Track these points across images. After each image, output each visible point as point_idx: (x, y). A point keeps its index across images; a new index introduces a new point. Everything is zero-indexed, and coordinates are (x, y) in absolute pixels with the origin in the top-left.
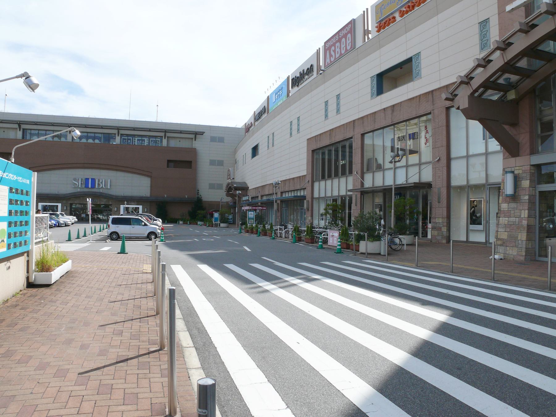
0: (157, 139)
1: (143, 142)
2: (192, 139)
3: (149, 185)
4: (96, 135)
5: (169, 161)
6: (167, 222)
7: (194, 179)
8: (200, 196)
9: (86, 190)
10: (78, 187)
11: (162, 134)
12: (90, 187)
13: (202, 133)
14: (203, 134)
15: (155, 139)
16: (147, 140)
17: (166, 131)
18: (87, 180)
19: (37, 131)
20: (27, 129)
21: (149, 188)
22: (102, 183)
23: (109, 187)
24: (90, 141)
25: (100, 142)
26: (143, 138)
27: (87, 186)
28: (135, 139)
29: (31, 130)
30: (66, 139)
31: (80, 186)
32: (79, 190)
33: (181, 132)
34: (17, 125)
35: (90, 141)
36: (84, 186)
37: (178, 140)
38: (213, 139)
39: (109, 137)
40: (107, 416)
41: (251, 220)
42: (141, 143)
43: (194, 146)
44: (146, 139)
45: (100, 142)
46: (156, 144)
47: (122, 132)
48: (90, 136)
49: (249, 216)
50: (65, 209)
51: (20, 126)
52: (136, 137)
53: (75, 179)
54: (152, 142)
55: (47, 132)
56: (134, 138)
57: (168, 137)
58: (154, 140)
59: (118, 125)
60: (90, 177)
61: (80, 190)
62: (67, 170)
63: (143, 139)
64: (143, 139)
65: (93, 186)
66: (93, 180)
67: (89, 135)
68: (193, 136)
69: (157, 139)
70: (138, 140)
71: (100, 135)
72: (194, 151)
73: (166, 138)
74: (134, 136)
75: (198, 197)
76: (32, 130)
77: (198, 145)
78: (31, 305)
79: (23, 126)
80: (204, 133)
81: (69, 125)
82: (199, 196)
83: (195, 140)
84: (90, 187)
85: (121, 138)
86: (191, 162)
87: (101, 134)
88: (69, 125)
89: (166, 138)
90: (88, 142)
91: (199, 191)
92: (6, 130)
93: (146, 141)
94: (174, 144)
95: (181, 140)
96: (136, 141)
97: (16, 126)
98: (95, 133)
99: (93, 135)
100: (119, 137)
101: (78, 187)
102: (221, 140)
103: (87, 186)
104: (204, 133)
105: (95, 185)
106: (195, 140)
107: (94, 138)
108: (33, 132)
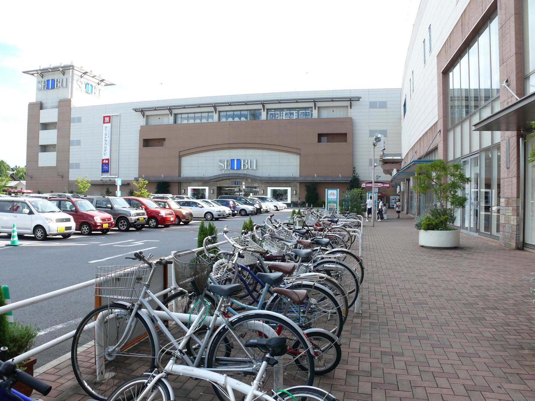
0: (306, 111)
1: (292, 116)
2: (347, 107)
3: (298, 164)
4: (242, 112)
5: (320, 136)
6: (293, 206)
7: (351, 155)
8: (357, 174)
9: (232, 172)
10: (224, 169)
11: (312, 105)
12: (236, 168)
13: (358, 99)
14: (359, 100)
15: (305, 111)
16: (296, 113)
17: (315, 101)
18: (232, 161)
19: (207, 114)
20: (178, 114)
21: (298, 167)
22: (247, 163)
23: (255, 168)
24: (230, 119)
25: (246, 120)
26: (292, 111)
27: (232, 168)
28: (282, 113)
29: (181, 114)
30: (213, 119)
31: (226, 168)
32: (223, 172)
33: (332, 100)
34: (213, 108)
35: (230, 119)
36: (229, 168)
37: (331, 109)
38: (373, 105)
39: (255, 115)
40: (386, 400)
41: (331, 204)
42: (290, 117)
43: (349, 114)
44: (294, 112)
45: (246, 120)
46: (307, 117)
47: (268, 106)
48: (243, 114)
49: (329, 197)
50: (212, 193)
51: (216, 108)
52: (285, 111)
53: (221, 161)
54: (302, 115)
55: (227, 113)
56: (281, 112)
57: (319, 108)
58: (304, 113)
59: (332, 97)
60: (236, 158)
61: (247, 172)
62: (270, 151)
63: (291, 112)
64: (291, 112)
65: (239, 168)
66: (239, 161)
67: (228, 113)
68: (348, 103)
69: (306, 111)
70: (286, 114)
71: (246, 112)
72: (349, 121)
73: (317, 109)
74: (282, 109)
75: (355, 176)
76: (182, 115)
77: (354, 113)
78: (502, 285)
79: (219, 109)
80: (361, 98)
81: (262, 102)
82: (355, 174)
83: (351, 108)
84: (236, 168)
85: (267, 113)
86: (345, 135)
87: (247, 111)
88: (262, 102)
89: (317, 109)
90: (202, 122)
91: (355, 169)
92: (161, 117)
93: (295, 114)
94: (325, 114)
95: (335, 109)
96: (284, 114)
97: (167, 112)
98: (241, 111)
99: (239, 113)
100: (265, 112)
101: (224, 169)
102: (383, 105)
103: (232, 168)
104: (361, 98)
105: (241, 166)
106: (351, 108)
107: (233, 117)
108: (183, 116)
